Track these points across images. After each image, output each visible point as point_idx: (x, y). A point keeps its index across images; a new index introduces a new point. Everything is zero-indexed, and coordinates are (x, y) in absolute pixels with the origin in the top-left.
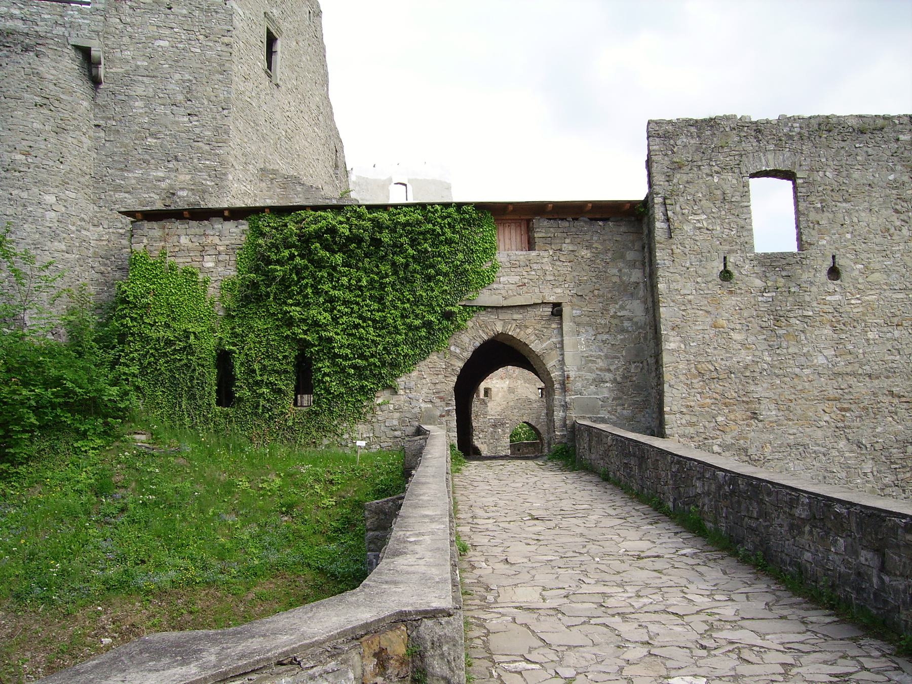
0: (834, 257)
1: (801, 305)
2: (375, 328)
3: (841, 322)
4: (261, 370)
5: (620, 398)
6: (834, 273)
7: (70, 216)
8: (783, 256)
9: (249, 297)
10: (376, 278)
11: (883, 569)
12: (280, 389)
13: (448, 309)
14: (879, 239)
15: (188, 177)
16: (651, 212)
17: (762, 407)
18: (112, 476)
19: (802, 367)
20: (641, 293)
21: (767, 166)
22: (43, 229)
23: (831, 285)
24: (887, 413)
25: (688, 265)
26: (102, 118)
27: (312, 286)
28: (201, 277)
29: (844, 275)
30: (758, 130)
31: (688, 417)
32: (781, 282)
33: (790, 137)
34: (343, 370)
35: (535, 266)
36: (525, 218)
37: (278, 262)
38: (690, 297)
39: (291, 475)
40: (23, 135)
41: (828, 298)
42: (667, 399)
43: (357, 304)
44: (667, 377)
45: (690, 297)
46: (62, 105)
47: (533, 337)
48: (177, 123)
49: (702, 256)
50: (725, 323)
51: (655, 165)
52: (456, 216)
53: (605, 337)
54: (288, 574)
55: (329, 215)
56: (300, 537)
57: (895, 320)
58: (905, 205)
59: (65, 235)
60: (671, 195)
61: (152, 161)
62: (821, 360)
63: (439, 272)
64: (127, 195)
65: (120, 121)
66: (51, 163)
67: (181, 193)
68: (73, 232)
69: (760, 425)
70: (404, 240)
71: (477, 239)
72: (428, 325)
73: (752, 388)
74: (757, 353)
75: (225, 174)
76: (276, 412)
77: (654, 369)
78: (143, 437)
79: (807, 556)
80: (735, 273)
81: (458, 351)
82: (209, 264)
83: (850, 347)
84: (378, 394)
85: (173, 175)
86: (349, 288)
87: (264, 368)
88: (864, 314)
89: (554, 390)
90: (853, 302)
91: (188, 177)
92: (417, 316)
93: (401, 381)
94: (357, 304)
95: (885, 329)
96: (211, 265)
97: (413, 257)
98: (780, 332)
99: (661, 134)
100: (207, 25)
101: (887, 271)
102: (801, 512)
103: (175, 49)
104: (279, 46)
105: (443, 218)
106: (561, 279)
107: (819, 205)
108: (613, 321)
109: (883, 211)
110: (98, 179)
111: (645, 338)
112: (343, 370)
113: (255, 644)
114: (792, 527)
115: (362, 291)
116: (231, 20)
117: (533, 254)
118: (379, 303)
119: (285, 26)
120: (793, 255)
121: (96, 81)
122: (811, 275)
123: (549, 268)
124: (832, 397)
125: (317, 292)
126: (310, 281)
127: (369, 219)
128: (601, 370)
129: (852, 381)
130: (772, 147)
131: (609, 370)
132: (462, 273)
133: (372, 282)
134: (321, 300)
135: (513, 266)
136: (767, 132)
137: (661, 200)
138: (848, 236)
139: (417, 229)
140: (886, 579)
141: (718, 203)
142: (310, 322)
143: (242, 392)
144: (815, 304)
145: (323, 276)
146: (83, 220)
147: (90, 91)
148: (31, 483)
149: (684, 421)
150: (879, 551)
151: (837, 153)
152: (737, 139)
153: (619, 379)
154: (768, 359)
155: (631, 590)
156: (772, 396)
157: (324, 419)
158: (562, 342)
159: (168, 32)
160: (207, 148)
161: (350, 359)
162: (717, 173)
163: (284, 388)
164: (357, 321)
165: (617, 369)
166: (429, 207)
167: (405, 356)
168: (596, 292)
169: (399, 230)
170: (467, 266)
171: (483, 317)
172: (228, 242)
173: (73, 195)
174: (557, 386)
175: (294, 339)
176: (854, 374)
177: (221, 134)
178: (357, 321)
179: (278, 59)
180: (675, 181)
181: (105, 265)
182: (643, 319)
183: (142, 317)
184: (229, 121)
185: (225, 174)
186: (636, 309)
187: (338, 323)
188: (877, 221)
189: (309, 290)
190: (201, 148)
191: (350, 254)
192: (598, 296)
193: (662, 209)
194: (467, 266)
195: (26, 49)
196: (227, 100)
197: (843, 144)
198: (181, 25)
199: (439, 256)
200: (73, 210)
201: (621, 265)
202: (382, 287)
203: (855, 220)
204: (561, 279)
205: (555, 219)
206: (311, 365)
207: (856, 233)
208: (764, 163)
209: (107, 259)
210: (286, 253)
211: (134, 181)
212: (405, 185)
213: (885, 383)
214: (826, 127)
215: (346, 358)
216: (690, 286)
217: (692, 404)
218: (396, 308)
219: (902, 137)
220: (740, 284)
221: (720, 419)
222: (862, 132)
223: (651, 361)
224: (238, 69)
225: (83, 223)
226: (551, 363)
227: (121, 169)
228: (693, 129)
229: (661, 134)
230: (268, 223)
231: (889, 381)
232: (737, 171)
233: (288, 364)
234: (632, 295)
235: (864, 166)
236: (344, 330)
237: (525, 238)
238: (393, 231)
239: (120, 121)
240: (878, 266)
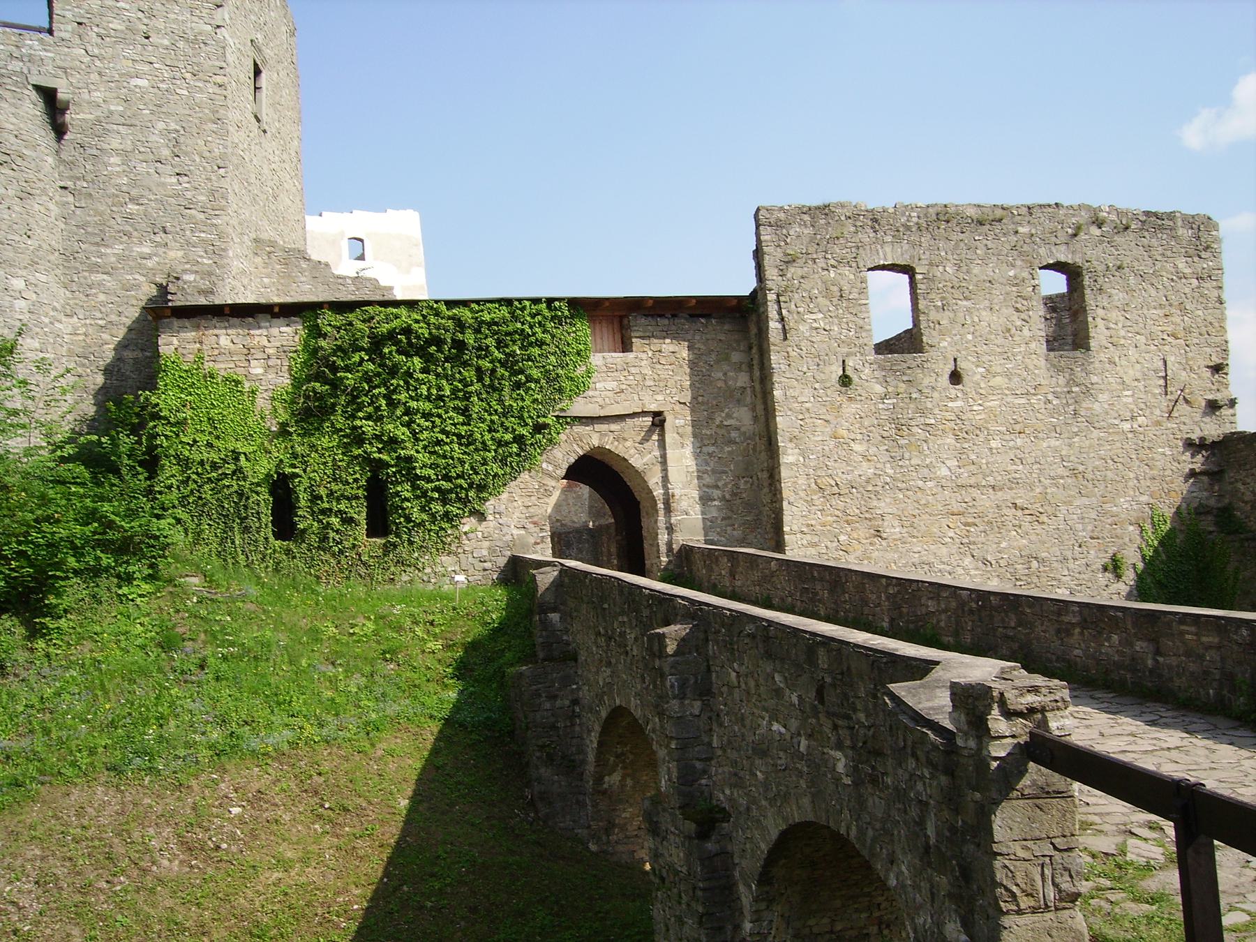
0: (955, 360)
1: (923, 412)
2: (460, 444)
3: (964, 431)
4: (327, 496)
5: (729, 518)
6: (956, 377)
7: (42, 304)
9: (309, 413)
10: (460, 386)
11: (1158, 652)
12: (352, 518)
13: (541, 420)
14: (1000, 341)
15: (180, 253)
16: (762, 310)
17: (886, 523)
18: (174, 626)
19: (925, 480)
20: (748, 400)
21: (885, 259)
22: (13, 322)
23: (953, 391)
24: (1010, 527)
25: (805, 369)
26: (70, 178)
27: (385, 396)
28: (247, 386)
29: (966, 379)
30: (875, 219)
31: (808, 537)
32: (902, 387)
33: (908, 228)
34: (424, 494)
35: (633, 370)
36: (622, 318)
37: (347, 369)
38: (807, 405)
39: (382, 617)
41: (950, 404)
43: (439, 416)
44: (786, 493)
45: (807, 405)
46: (25, 163)
47: (632, 451)
48: (164, 185)
49: (820, 361)
50: (845, 433)
51: (766, 257)
52: (547, 313)
53: (711, 449)
54: (413, 728)
55: (403, 311)
56: (415, 686)
57: (1018, 427)
58: (1025, 303)
59: (38, 330)
60: (785, 291)
61: (135, 234)
62: (944, 472)
63: (529, 379)
64: (105, 277)
65: (93, 181)
66: (17, 238)
67: (187, 277)
68: (46, 326)
69: (884, 543)
70: (489, 341)
71: (569, 339)
72: (519, 439)
73: (875, 503)
74: (878, 466)
76: (347, 544)
77: (766, 484)
78: (195, 580)
79: (1077, 652)
81: (550, 468)
82: (257, 369)
83: (973, 457)
84: (463, 521)
85: (161, 250)
86: (428, 398)
87: (331, 493)
88: (986, 422)
89: (657, 511)
90: (975, 408)
91: (180, 253)
92: (507, 429)
93: (490, 506)
94: (439, 416)
95: (1007, 437)
96: (260, 371)
97: (500, 361)
100: (194, 60)
101: (1008, 375)
103: (156, 90)
105: (533, 316)
106: (662, 384)
107: (939, 304)
108: (719, 431)
109: (1004, 310)
110: (69, 256)
111: (754, 450)
112: (424, 494)
114: (1058, 631)
115: (443, 401)
116: (224, 54)
117: (631, 355)
118: (462, 415)
121: (59, 130)
122: (933, 380)
123: (648, 371)
124: (956, 511)
125: (392, 404)
126: (383, 390)
127: (449, 318)
128: (708, 487)
129: (975, 493)
130: (889, 239)
131: (717, 487)
132: (554, 379)
133: (454, 391)
134: (398, 413)
135: (609, 370)
136: (883, 222)
137: (775, 297)
138: (970, 337)
139: (504, 328)
140: (1161, 659)
142: (385, 438)
143: (304, 521)
145: (399, 385)
146: (54, 309)
147: (54, 144)
148: (79, 639)
149: (805, 542)
150: (1154, 641)
151: (956, 246)
152: (853, 229)
153: (728, 497)
154: (890, 472)
156: (895, 511)
157: (403, 551)
158: (664, 456)
159: (146, 68)
160: (202, 216)
161: (432, 481)
162: (833, 266)
163: (356, 516)
164: (441, 436)
165: (726, 485)
166: (516, 303)
167: (494, 476)
168: (700, 399)
169: (484, 330)
170: (560, 371)
171: (578, 429)
172: (278, 344)
173: (43, 278)
174: (661, 506)
175: (367, 460)
176: (977, 486)
178: (441, 436)
180: (789, 275)
181: (83, 365)
182: (751, 428)
183: (178, 435)
185: (223, 250)
186: (742, 417)
187: (417, 440)
188: (997, 321)
189: (383, 402)
190: (194, 217)
191: (428, 359)
192: (703, 404)
193: (776, 307)
194: (560, 371)
196: (223, 156)
197: (962, 236)
198: (162, 60)
199: (529, 359)
200: (44, 298)
201: (726, 368)
202: (467, 398)
203: (976, 319)
204: (662, 384)
205: (652, 316)
206: (386, 489)
207: (977, 334)
208: (881, 255)
209: (86, 358)
210: (356, 358)
211: (113, 259)
212: (361, 240)
213: (1008, 495)
214: (941, 218)
215: (429, 480)
216: (808, 392)
217: (813, 522)
218: (483, 420)
219: (1021, 229)
220: (860, 391)
221: (842, 538)
222: (981, 223)
223: (765, 475)
224: (233, 116)
225: (55, 313)
227: (97, 244)
228: (806, 217)
230: (327, 320)
231: (1012, 493)
232: (854, 265)
233: (358, 488)
234: (738, 401)
235: (984, 261)
236: (425, 447)
237: (618, 337)
238: (478, 331)
239: (93, 181)
240: (999, 369)
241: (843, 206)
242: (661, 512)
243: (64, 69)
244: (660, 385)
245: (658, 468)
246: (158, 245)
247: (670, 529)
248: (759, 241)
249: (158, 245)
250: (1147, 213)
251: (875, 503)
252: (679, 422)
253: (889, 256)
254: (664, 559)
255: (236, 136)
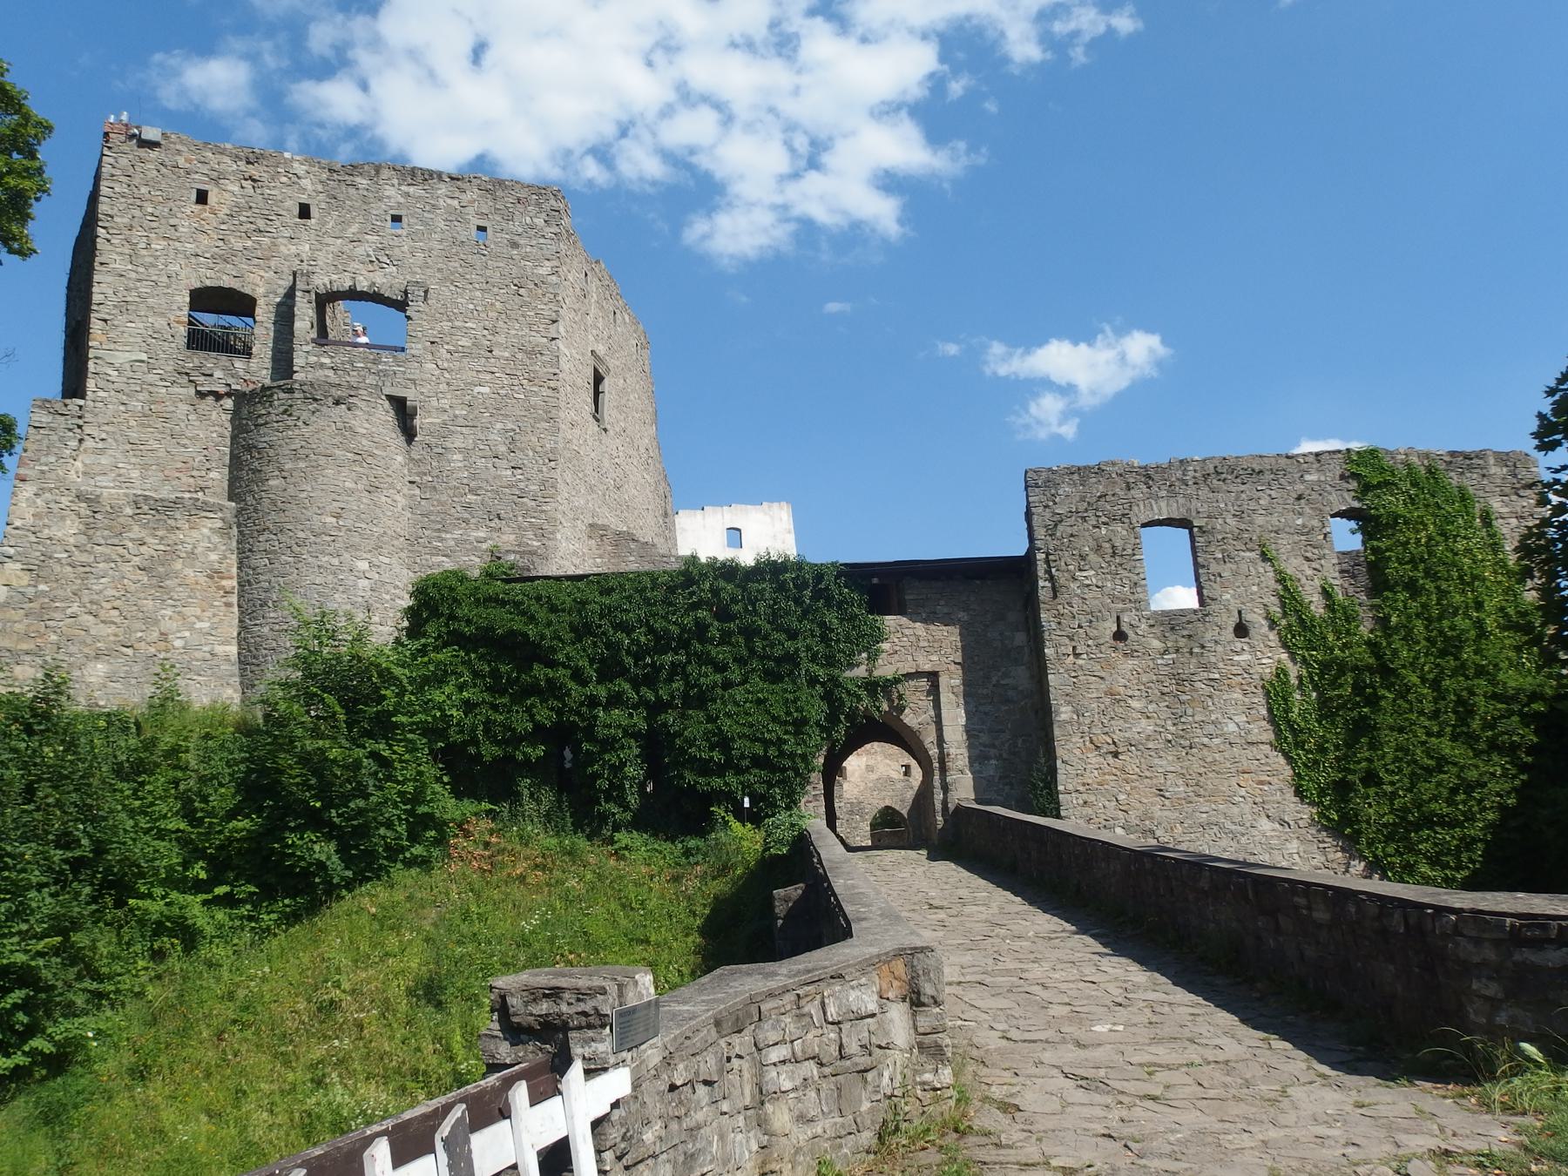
1: (1206, 667)
7: (384, 583)
8: (1182, 613)
15: (513, 537)
23: (1239, 644)
26: (418, 474)
29: (1252, 632)
30: (1147, 475)
32: (1182, 642)
35: (907, 632)
40: (334, 496)
42: (1061, 777)
49: (1094, 617)
50: (1121, 690)
53: (988, 708)
62: (1232, 727)
75: (552, 533)
80: (1130, 633)
91: (513, 537)
98: (1184, 697)
99: (1038, 483)
102: (1204, 884)
104: (606, 385)
113: (856, 952)
119: (612, 363)
120: (1195, 611)
121: (409, 433)
130: (1164, 493)
131: (993, 746)
141: (1108, 558)
144: (1221, 665)
146: (396, 587)
155: (1046, 966)
158: (938, 716)
159: (488, 377)
173: (387, 560)
177: (548, 486)
179: (607, 399)
184: (557, 474)
195: (337, 403)
197: (1243, 487)
200: (386, 577)
221: (1122, 797)
224: (566, 415)
226: (929, 739)
229: (1038, 483)
235: (1268, 511)
241: (1114, 464)
242: (937, 772)
243: (414, 381)
244: (934, 647)
245: (933, 727)
246: (493, 529)
247: (945, 788)
248: (1028, 503)
249: (493, 529)
250: (1453, 454)
251: (1157, 761)
252: (951, 681)
253: (1164, 510)
254: (940, 818)
255: (566, 432)
